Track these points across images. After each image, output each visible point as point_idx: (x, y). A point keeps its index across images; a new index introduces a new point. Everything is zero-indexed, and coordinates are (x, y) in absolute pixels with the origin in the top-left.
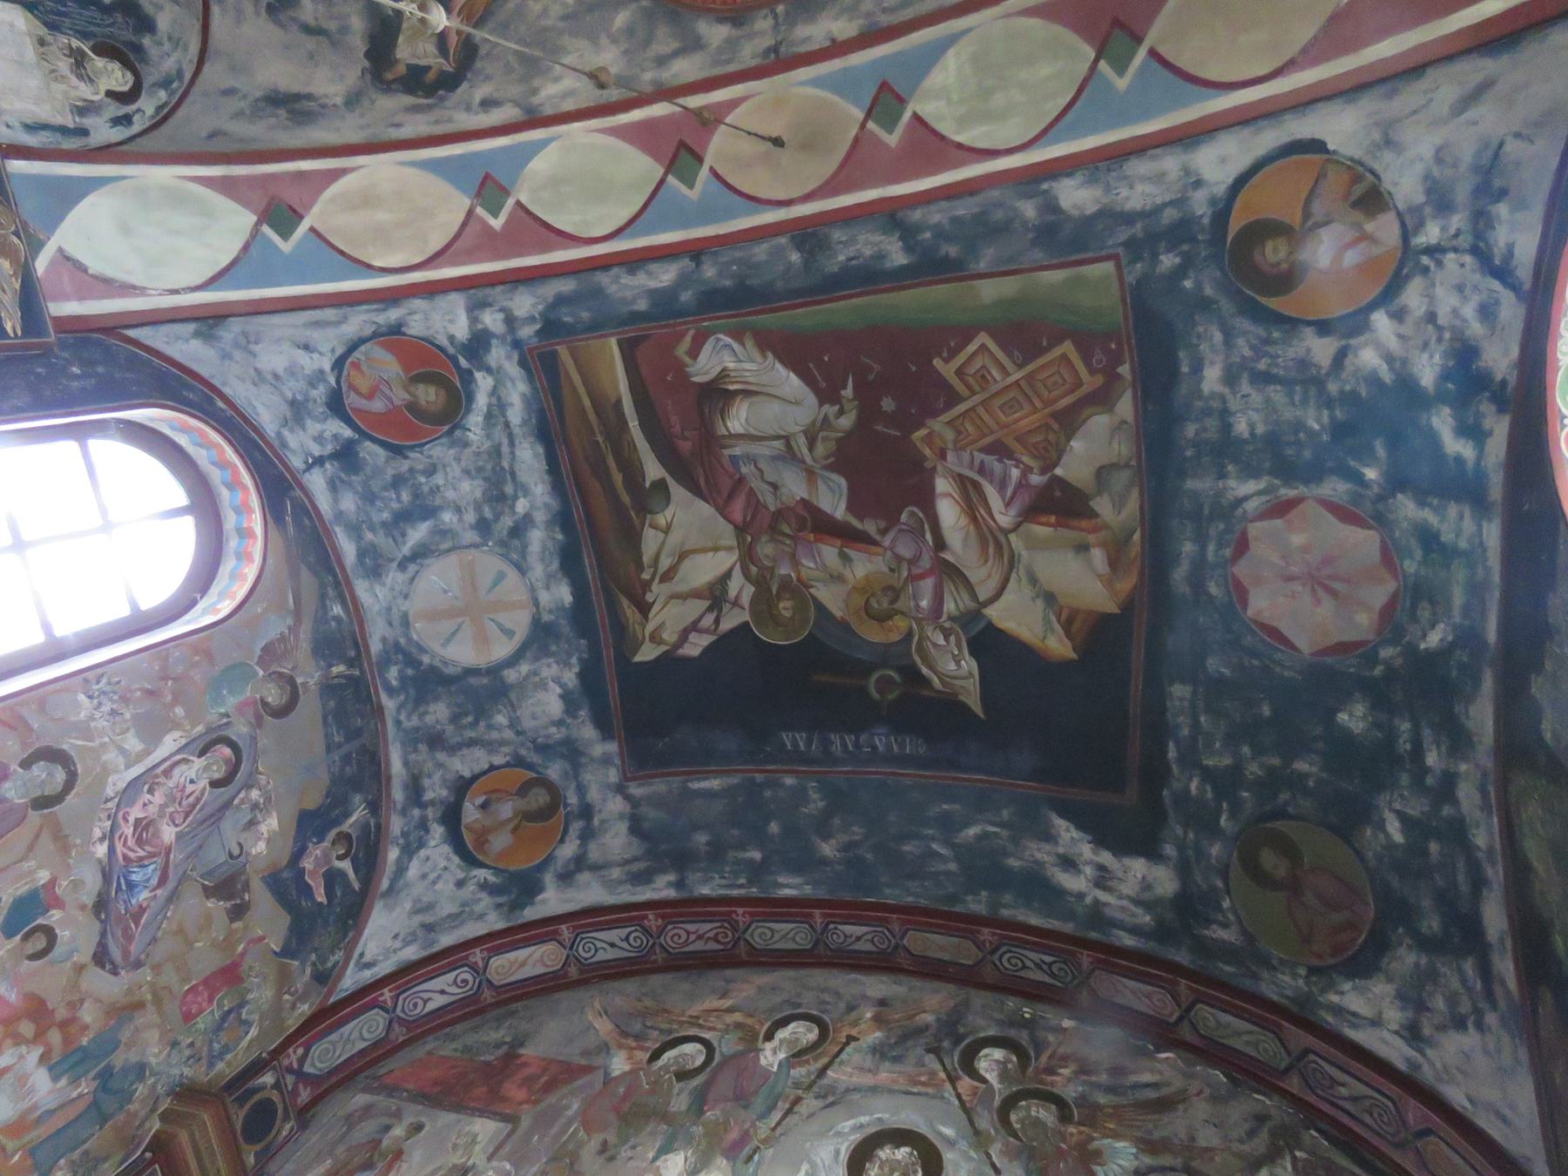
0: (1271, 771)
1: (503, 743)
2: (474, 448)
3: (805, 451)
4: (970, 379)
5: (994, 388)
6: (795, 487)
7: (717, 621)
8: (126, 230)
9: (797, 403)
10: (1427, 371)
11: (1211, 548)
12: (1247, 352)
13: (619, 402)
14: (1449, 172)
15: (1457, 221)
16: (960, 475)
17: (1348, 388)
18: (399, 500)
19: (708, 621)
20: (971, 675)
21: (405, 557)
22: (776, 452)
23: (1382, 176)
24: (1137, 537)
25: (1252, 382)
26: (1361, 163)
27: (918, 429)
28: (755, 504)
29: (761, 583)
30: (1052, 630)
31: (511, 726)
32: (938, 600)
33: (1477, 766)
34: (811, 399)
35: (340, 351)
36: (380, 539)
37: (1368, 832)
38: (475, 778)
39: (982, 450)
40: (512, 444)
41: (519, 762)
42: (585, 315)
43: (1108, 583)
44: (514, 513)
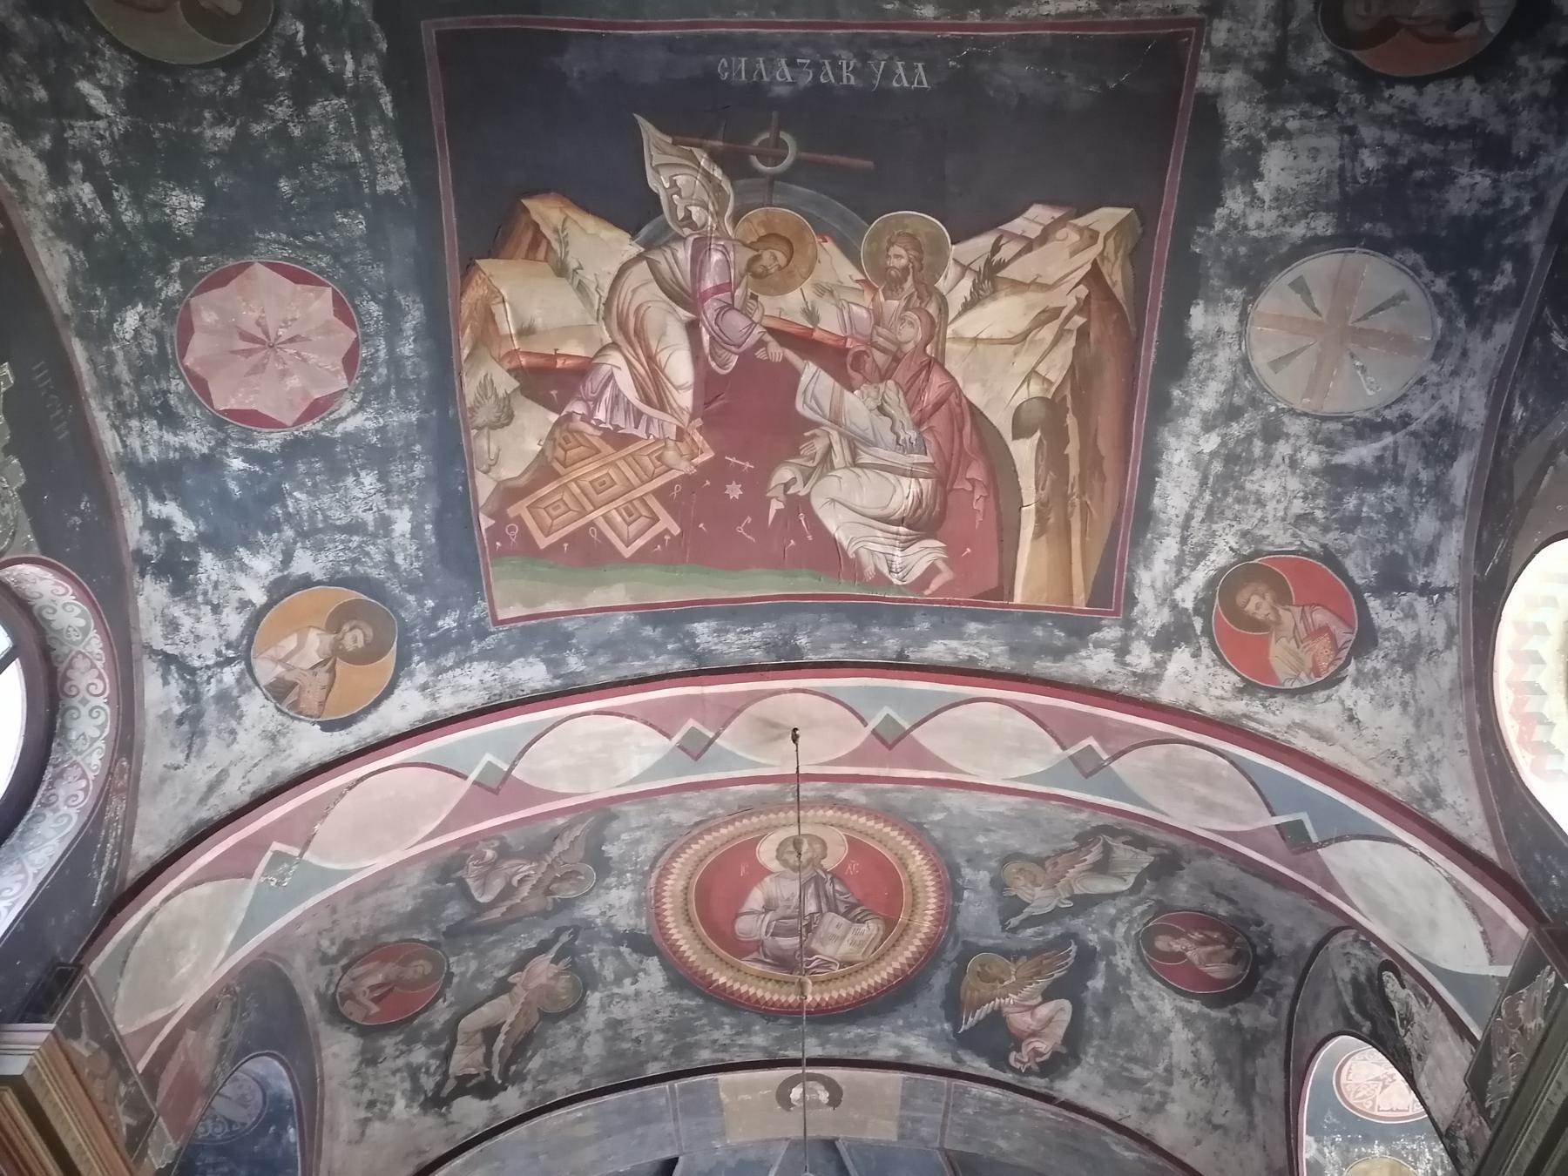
0: (259, 115)
1: (1385, 122)
2: (1237, 527)
3: (837, 447)
4: (644, 512)
5: (620, 502)
6: (857, 406)
7: (996, 248)
8: (1433, 925)
9: (833, 500)
10: (209, 565)
11: (382, 354)
12: (371, 549)
13: (1037, 535)
14: (223, 725)
15: (211, 690)
16: (663, 409)
17: (275, 535)
18: (1362, 501)
19: (1008, 250)
20: (656, 170)
21: (1394, 432)
22: (872, 450)
23: (275, 711)
24: (466, 352)
25: (364, 524)
26: (293, 718)
27: (705, 463)
28: (911, 394)
29: (926, 289)
30: (556, 231)
31: (1358, 145)
32: (698, 261)
33: (36, 205)
34: (817, 503)
35: (1322, 694)
36: (1413, 464)
37: (121, 79)
38: (1457, 73)
39: (636, 439)
40: (1189, 517)
41: (1371, 82)
42: (1039, 632)
43: (495, 292)
44: (1224, 436)
